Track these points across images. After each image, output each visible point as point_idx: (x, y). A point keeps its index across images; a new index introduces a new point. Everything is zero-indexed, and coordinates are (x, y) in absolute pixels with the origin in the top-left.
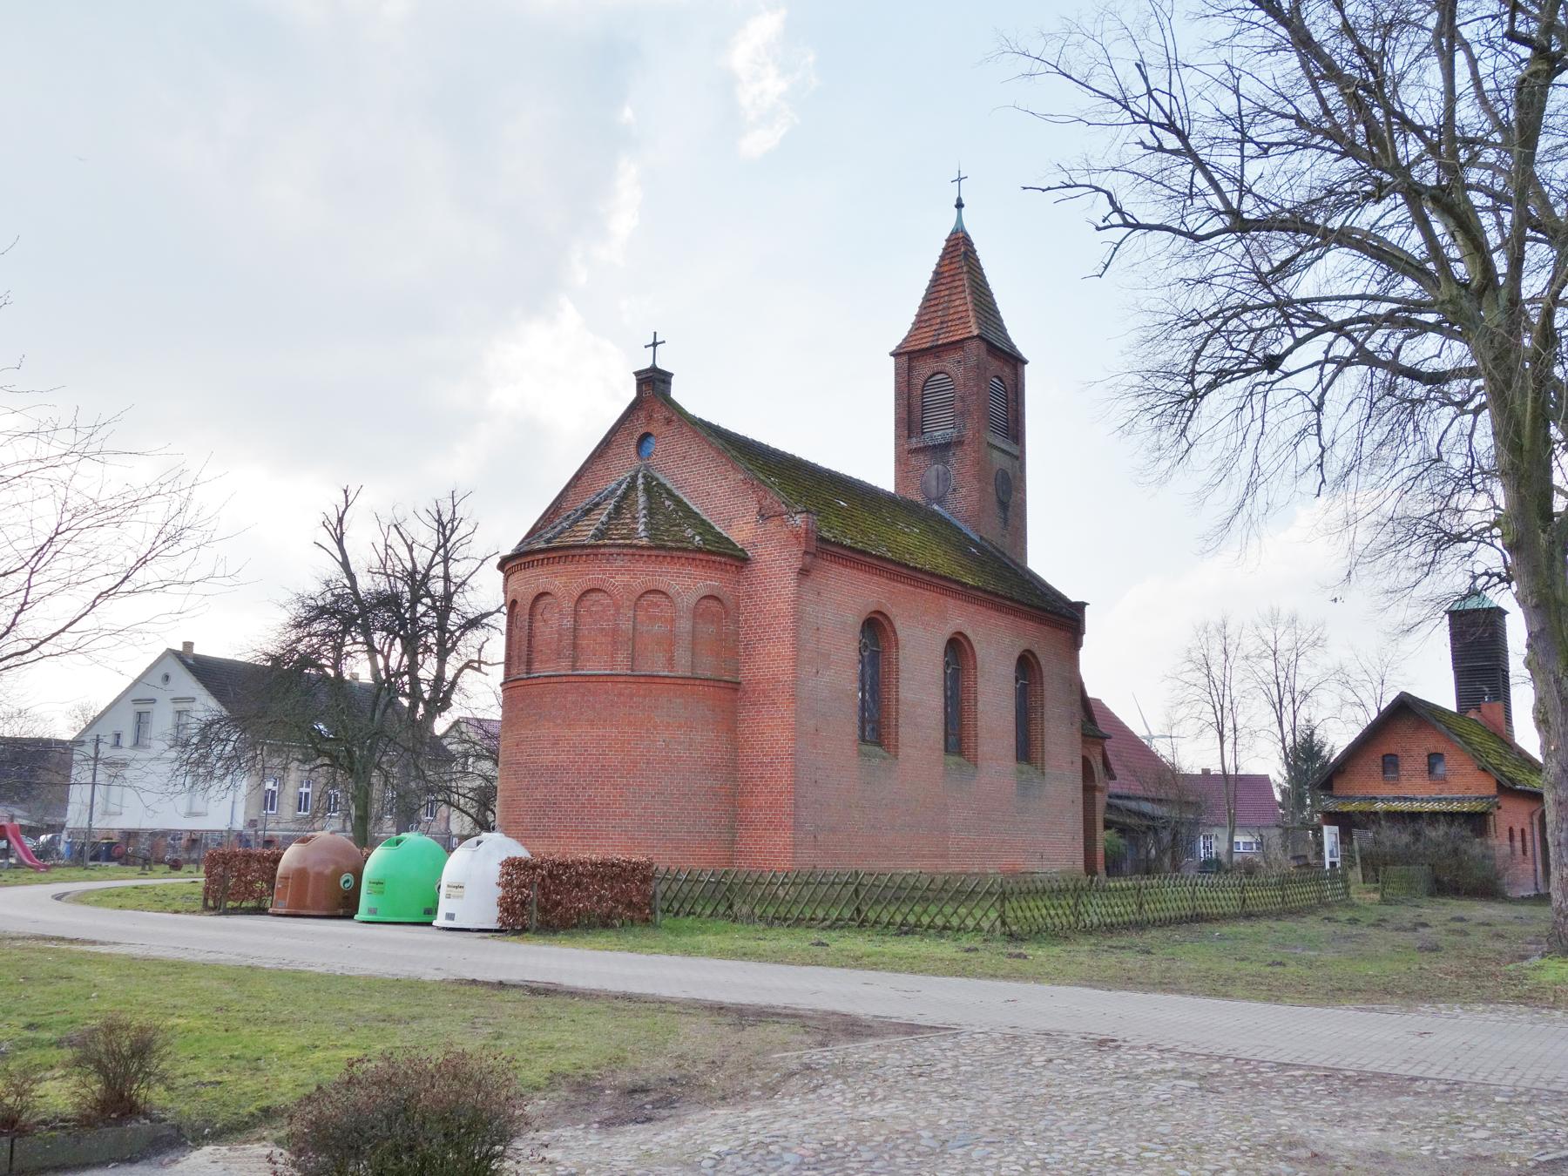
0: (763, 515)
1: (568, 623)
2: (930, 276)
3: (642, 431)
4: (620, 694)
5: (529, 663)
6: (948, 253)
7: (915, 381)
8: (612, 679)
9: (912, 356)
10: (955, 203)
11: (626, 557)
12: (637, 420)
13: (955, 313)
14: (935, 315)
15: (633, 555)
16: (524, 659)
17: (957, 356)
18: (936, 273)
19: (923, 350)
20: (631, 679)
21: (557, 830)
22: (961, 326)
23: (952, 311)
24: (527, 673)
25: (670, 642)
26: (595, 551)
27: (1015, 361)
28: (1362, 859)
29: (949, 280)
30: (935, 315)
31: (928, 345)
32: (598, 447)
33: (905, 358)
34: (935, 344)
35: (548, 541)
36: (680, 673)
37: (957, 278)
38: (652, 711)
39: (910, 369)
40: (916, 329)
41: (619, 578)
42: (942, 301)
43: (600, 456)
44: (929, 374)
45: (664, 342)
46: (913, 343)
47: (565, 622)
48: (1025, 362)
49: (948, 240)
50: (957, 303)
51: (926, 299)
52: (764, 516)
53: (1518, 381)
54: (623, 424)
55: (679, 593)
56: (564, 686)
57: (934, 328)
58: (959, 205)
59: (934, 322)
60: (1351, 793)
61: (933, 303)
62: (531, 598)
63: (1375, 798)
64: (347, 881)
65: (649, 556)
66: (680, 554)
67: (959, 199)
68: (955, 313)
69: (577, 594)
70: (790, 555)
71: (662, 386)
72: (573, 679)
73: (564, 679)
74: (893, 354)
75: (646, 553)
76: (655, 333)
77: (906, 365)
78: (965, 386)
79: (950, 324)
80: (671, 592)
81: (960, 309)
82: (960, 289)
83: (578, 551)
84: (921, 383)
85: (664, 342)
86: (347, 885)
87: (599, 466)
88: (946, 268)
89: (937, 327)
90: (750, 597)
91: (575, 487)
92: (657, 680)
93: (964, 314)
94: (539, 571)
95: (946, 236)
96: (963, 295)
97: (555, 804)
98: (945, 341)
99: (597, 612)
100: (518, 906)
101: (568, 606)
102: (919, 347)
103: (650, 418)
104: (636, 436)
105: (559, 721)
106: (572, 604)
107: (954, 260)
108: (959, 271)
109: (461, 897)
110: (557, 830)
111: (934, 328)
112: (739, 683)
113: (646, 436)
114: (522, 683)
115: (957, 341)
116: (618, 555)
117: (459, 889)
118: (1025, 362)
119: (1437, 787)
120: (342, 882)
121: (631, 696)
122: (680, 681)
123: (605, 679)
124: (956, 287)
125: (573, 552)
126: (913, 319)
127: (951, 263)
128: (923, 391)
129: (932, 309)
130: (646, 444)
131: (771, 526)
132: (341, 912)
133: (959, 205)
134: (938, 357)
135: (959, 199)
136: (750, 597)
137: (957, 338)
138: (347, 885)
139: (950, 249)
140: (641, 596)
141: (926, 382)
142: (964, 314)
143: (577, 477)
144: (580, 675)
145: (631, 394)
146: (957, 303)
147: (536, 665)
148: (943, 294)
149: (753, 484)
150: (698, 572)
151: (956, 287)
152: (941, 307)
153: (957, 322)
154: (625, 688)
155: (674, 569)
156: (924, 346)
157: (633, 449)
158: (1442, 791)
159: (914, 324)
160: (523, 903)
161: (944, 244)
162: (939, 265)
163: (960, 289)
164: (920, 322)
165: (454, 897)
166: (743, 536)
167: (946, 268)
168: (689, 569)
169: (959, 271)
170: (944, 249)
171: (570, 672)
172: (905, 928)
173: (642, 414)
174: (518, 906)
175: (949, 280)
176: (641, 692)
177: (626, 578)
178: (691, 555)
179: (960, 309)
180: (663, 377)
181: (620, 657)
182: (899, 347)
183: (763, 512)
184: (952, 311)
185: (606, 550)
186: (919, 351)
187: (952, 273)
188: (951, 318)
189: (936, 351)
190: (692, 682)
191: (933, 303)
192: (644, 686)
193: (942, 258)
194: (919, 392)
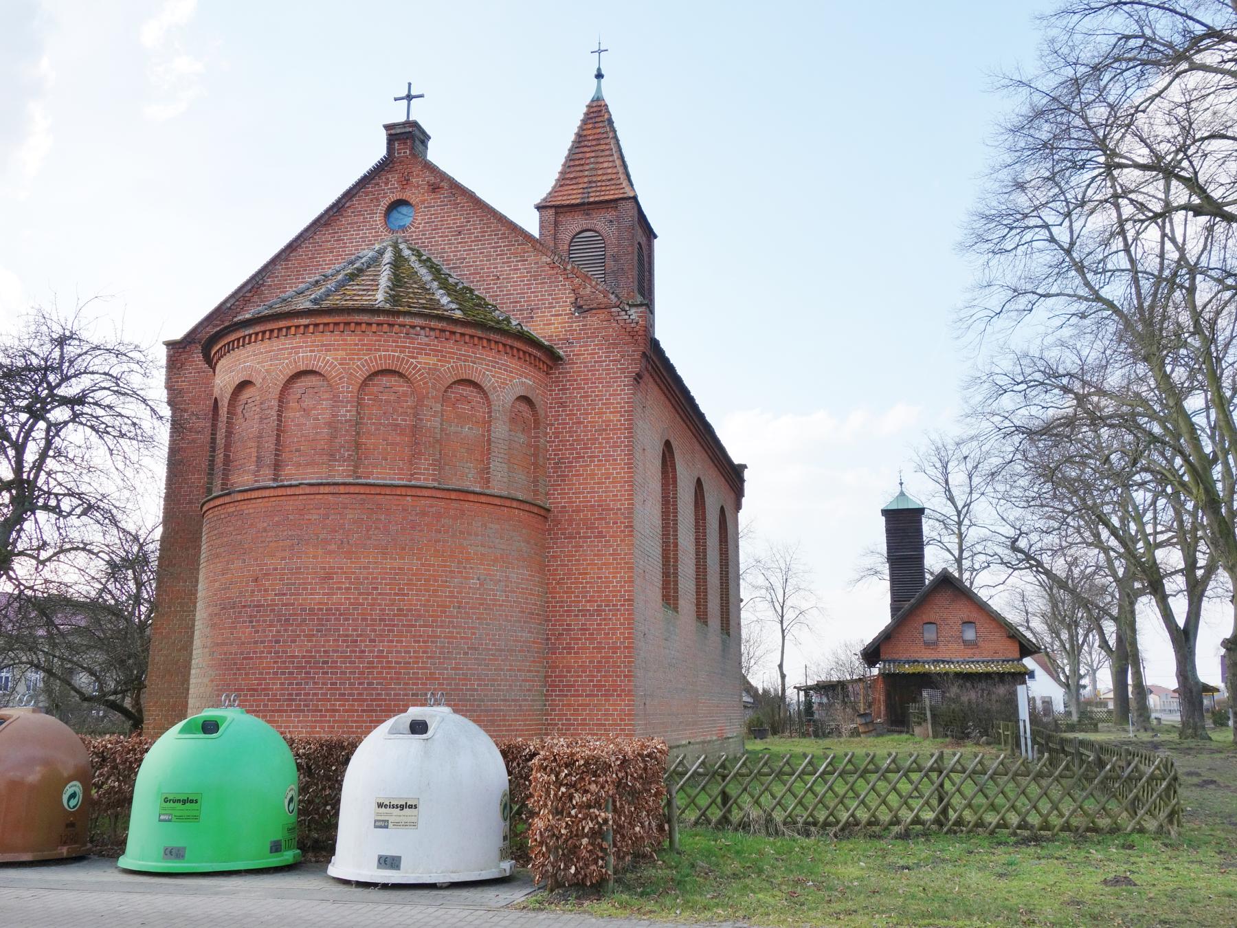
0: (580, 307)
1: (346, 412)
2: (572, 137)
3: (393, 197)
4: (424, 514)
5: (277, 466)
6: (591, 118)
7: (562, 236)
8: (414, 492)
9: (560, 210)
10: (595, 72)
11: (432, 333)
12: (386, 184)
13: (604, 174)
14: (581, 174)
15: (442, 331)
16: (269, 459)
17: (611, 215)
18: (579, 135)
19: (573, 205)
20: (439, 494)
21: (329, 700)
22: (613, 187)
23: (600, 172)
24: (275, 480)
25: (484, 448)
26: (391, 319)
27: (650, 234)
28: (934, 716)
29: (594, 143)
30: (581, 174)
31: (578, 201)
32: (327, 211)
33: (552, 211)
34: (586, 200)
35: (315, 301)
36: (496, 492)
37: (602, 142)
38: (465, 539)
39: (556, 224)
40: (561, 186)
41: (422, 359)
42: (588, 161)
43: (326, 224)
44: (578, 230)
45: (421, 96)
46: (560, 198)
47: (343, 411)
48: (655, 237)
49: (589, 106)
50: (606, 165)
51: (570, 158)
52: (581, 308)
53: (1163, 289)
54: (364, 187)
55: (494, 388)
56: (341, 499)
57: (581, 186)
58: (599, 76)
59: (580, 180)
60: (896, 657)
61: (577, 163)
62: (282, 379)
63: (917, 661)
64: (73, 796)
65: (462, 335)
66: (498, 338)
67: (599, 69)
68: (604, 174)
69: (361, 375)
70: (623, 356)
71: (421, 147)
72: (357, 489)
73: (342, 489)
74: (539, 208)
75: (459, 330)
76: (410, 84)
77: (552, 219)
78: (619, 245)
79: (599, 184)
80: (486, 385)
81: (609, 171)
82: (607, 153)
83: (365, 318)
84: (569, 239)
85: (421, 96)
86: (73, 802)
87: (325, 236)
88: (589, 132)
89: (585, 185)
90: (563, 405)
91: (286, 260)
92: (471, 497)
93: (614, 176)
94: (298, 341)
95: (588, 101)
96: (611, 159)
97: (324, 662)
98: (597, 199)
99: (387, 401)
100: (585, 841)
101: (347, 390)
102: (568, 202)
103: (405, 182)
104: (384, 203)
105: (333, 547)
106: (354, 388)
107: (597, 125)
108: (605, 136)
109: (414, 825)
110: (329, 700)
111: (581, 186)
112: (548, 510)
113: (401, 203)
114: (266, 493)
115: (611, 201)
116: (423, 328)
117: (407, 811)
118: (655, 237)
119: (970, 651)
120: (65, 797)
121: (439, 516)
122: (497, 501)
123: (404, 491)
124: (603, 151)
125: (357, 318)
126: (557, 176)
127: (595, 128)
128: (570, 246)
129: (578, 168)
130: (395, 214)
131: (593, 321)
132: (64, 851)
133: (599, 76)
134: (587, 214)
135: (599, 69)
136: (563, 405)
137: (611, 197)
138: (73, 802)
139: (592, 115)
140: (449, 387)
141: (573, 238)
142: (614, 176)
143: (292, 247)
144: (367, 485)
145: (379, 151)
146: (606, 165)
147: (289, 470)
148: (588, 155)
149: (565, 269)
150: (513, 364)
151: (603, 151)
152: (587, 167)
153: (608, 183)
154: (431, 506)
155: (489, 356)
156: (573, 202)
157: (378, 218)
158: (974, 654)
159: (558, 180)
160: (596, 834)
161: (585, 110)
162: (581, 128)
163: (607, 153)
164: (565, 179)
165: (397, 824)
166: (551, 330)
167: (589, 132)
168: (505, 359)
169: (605, 136)
170: (586, 114)
171: (351, 480)
172: (1026, 833)
173: (394, 178)
174: (585, 841)
175: (594, 143)
176: (452, 512)
177: (432, 360)
178: (509, 342)
179: (609, 171)
180: (422, 137)
181: (424, 464)
182: (545, 200)
183: (582, 303)
184: (600, 172)
185: (408, 320)
186: (568, 206)
187: (596, 137)
188: (599, 178)
189: (585, 208)
190: (508, 503)
191: (577, 163)
192: (455, 505)
193: (584, 122)
194: (566, 247)
